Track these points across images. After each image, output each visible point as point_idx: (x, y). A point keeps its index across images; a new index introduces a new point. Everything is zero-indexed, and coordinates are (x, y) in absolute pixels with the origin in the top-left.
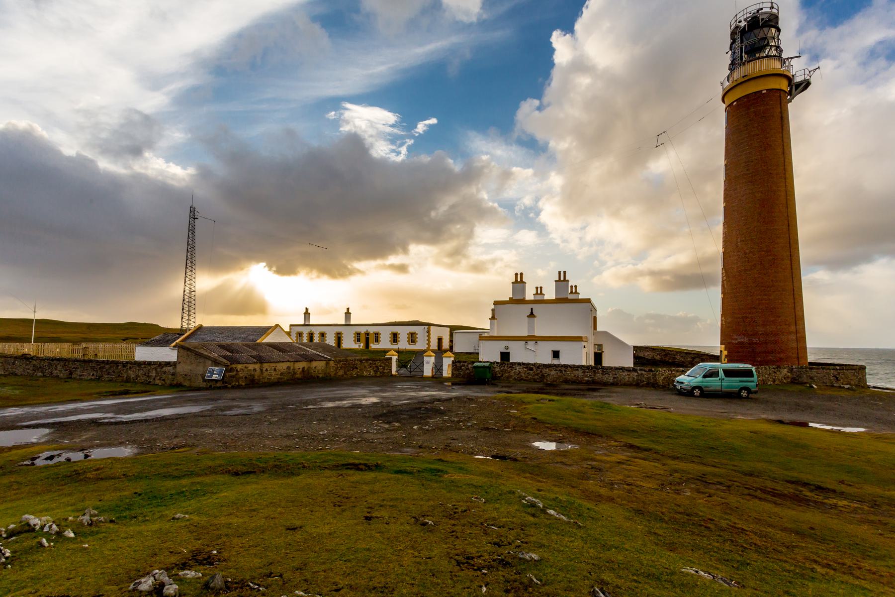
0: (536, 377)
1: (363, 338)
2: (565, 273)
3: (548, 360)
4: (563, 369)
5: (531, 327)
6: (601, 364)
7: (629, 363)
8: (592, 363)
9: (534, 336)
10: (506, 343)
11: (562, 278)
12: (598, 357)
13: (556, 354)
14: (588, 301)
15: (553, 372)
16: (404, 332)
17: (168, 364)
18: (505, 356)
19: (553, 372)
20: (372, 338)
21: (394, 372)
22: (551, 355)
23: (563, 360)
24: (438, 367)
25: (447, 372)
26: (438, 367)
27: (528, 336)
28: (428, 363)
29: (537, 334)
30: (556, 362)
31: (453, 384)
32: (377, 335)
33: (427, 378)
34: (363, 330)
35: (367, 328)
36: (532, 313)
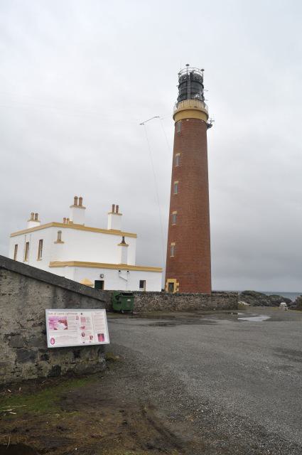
0: (170, 306)
3: (135, 287)
5: (124, 256)
9: (126, 265)
13: (142, 284)
18: (99, 284)
30: (142, 290)
36: (123, 242)
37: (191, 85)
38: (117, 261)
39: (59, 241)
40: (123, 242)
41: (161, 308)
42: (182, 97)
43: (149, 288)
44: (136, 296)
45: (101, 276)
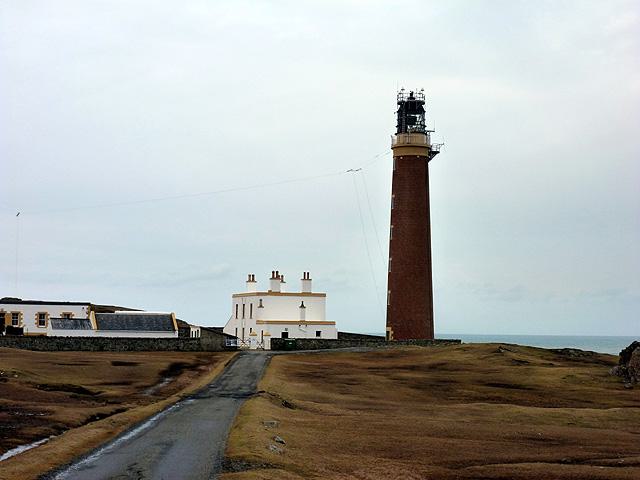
5: (303, 315)
13: (318, 333)
18: (285, 335)
37: (410, 110)
39: (261, 306)
42: (401, 129)
43: (323, 336)
45: (286, 329)
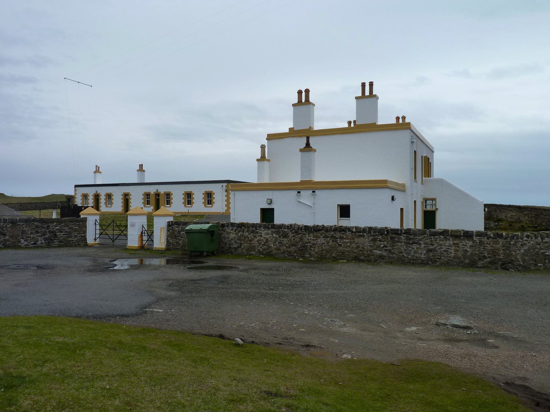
0: (293, 249)
1: (153, 200)
2: (371, 84)
3: (331, 219)
4: (338, 235)
5: (307, 167)
6: (433, 226)
7: (477, 224)
8: (420, 226)
9: (310, 182)
10: (269, 194)
11: (367, 93)
12: (430, 217)
13: (345, 211)
14: (402, 125)
15: (321, 240)
16: (198, 194)
17: (468, 235)
18: (267, 214)
19: (321, 240)
20: (162, 199)
21: (90, 240)
22: (335, 212)
23: (353, 222)
24: (148, 231)
25: (160, 241)
26: (148, 231)
27: (302, 183)
28: (133, 225)
29: (317, 178)
30: (344, 223)
31: (168, 262)
32: (168, 195)
33: (133, 250)
34: (152, 190)
35: (157, 187)
36: (308, 145)
38: (296, 178)
40: (308, 145)
41: (274, 252)
44: (229, 230)
